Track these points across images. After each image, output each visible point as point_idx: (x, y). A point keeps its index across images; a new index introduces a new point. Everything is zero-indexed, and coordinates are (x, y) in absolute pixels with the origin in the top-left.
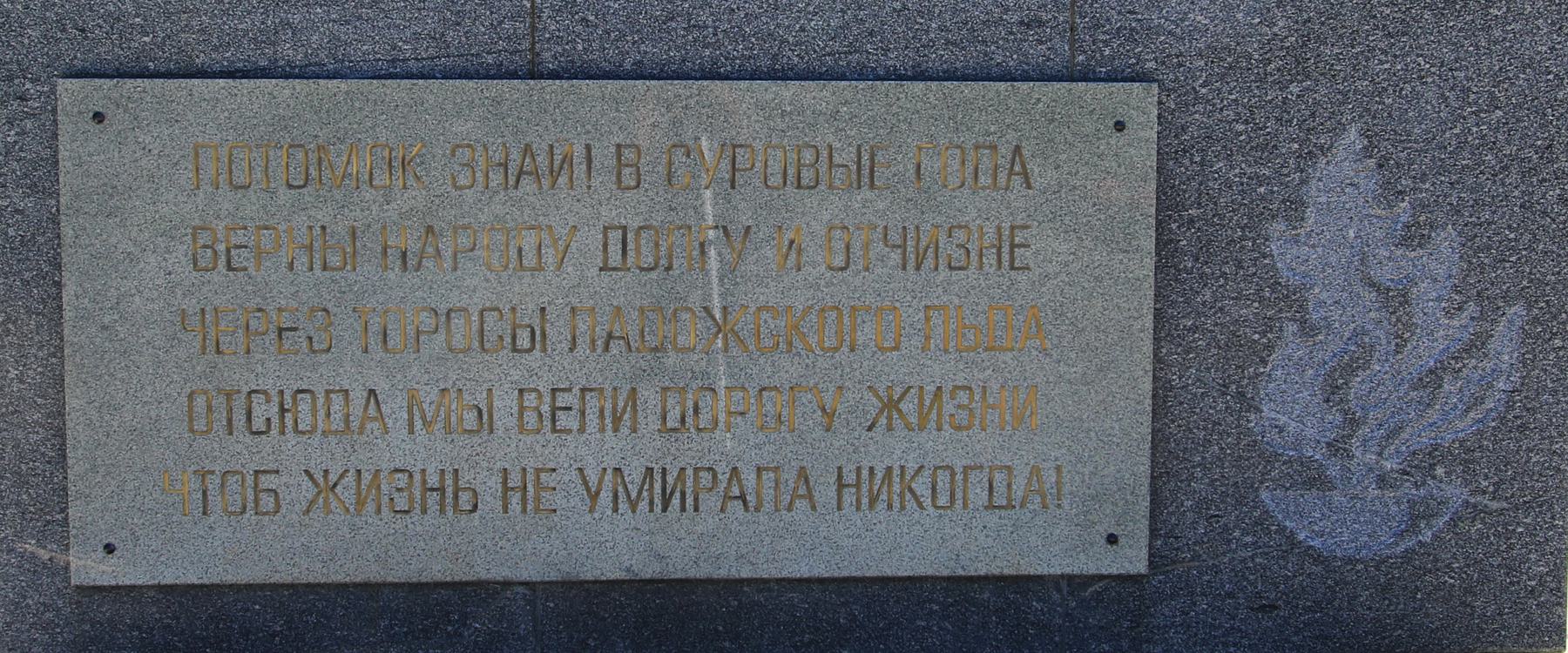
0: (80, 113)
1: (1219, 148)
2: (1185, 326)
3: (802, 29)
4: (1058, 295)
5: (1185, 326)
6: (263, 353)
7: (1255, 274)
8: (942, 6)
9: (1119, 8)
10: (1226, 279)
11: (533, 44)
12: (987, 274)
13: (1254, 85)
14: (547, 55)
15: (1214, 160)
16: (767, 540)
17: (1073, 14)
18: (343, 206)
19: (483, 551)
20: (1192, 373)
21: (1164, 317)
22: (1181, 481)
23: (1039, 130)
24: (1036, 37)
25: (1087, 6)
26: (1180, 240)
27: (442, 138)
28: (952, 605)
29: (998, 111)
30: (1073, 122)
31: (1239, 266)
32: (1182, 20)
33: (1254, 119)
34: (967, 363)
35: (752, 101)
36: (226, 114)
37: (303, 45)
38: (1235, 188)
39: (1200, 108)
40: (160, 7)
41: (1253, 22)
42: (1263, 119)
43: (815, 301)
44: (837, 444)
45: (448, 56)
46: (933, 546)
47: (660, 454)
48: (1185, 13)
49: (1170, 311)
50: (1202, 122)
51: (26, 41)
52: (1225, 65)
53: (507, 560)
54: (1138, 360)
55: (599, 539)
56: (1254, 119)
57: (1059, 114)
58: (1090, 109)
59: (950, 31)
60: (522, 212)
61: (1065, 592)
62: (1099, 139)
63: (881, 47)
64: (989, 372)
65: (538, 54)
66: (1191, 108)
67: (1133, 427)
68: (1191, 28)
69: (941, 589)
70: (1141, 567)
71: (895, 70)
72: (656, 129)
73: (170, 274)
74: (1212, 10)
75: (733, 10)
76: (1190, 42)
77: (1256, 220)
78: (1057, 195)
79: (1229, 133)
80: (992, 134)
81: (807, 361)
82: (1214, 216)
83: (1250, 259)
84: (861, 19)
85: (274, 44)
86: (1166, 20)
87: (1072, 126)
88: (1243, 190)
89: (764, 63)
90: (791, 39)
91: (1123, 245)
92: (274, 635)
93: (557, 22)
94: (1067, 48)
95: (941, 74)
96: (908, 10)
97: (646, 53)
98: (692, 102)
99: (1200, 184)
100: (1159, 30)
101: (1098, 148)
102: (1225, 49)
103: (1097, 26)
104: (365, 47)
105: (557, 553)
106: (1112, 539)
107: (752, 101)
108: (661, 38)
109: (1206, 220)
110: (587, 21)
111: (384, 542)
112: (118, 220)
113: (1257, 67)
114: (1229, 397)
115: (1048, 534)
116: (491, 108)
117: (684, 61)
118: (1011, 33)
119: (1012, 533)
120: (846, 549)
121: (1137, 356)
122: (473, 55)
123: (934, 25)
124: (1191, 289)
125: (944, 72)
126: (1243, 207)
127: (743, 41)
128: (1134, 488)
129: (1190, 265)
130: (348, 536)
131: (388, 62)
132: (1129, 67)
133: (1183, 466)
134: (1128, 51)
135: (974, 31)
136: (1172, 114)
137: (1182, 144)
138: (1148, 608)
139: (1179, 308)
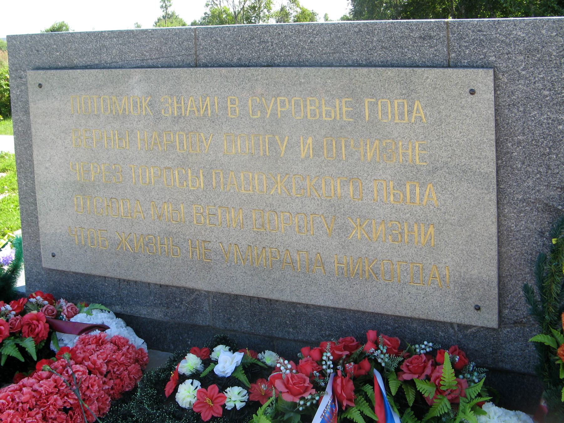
0: (34, 84)
1: (534, 104)
2: (518, 199)
3: (311, 42)
4: (443, 178)
5: (518, 199)
6: (99, 182)
7: (558, 173)
8: (379, 30)
9: (473, 29)
10: (541, 174)
11: (196, 51)
12: (405, 165)
13: (553, 69)
14: (202, 56)
15: (532, 110)
16: (304, 286)
17: (448, 32)
18: (123, 122)
19: (183, 274)
20: (522, 224)
21: (505, 193)
22: (518, 281)
23: (428, 93)
24: (428, 44)
25: (455, 28)
26: (513, 153)
27: (158, 94)
28: (397, 328)
29: (406, 83)
30: (447, 89)
31: (548, 168)
32: (509, 35)
33: (554, 88)
34: (397, 210)
35: (286, 77)
36: (81, 84)
37: (110, 55)
38: (544, 126)
39: (522, 82)
40: (62, 41)
41: (552, 35)
42: (560, 89)
43: (320, 174)
44: (334, 244)
45: (163, 57)
46: (384, 299)
47: (253, 240)
48: (511, 31)
49: (509, 190)
50: (523, 89)
51: (21, 56)
52: (536, 59)
53: (193, 279)
54: (488, 216)
55: (230, 275)
56: (554, 88)
57: (439, 85)
58: (455, 82)
59: (384, 42)
60: (191, 126)
61: (456, 330)
62: (461, 98)
63: (350, 50)
64: (408, 215)
65: (198, 56)
66: (517, 82)
67: (487, 251)
68: (515, 39)
69: (392, 319)
70: (493, 323)
71: (357, 61)
72: (244, 90)
73: (66, 148)
74: (527, 29)
75: (280, 34)
76: (514, 46)
77: (558, 143)
78: (440, 127)
79: (539, 96)
80: (403, 94)
81: (318, 202)
82: (532, 140)
83: (555, 165)
84: (339, 37)
85: (100, 54)
86: (500, 35)
87: (446, 91)
88: (549, 127)
89: (295, 58)
90: (306, 47)
91: (477, 154)
92: (112, 297)
93: (205, 42)
94: (445, 50)
95: (380, 63)
96: (362, 32)
97: (242, 54)
98: (259, 77)
99: (524, 123)
100: (496, 40)
101: (461, 103)
102: (535, 50)
103: (461, 38)
104: (132, 55)
105: (213, 279)
106: (478, 308)
107: (286, 77)
108: (248, 48)
109: (528, 143)
110: (217, 41)
111: (146, 265)
112: (48, 126)
113: (555, 59)
114: (544, 239)
115: (442, 301)
116: (176, 81)
117: (259, 58)
118: (415, 42)
119: (424, 298)
120: (341, 295)
121: (488, 214)
122: (172, 57)
123: (375, 39)
124: (521, 179)
125: (382, 62)
126: (549, 136)
127: (285, 48)
128: (489, 283)
129: (519, 166)
130: (133, 261)
131: (140, 60)
132: (480, 60)
133: (519, 273)
134: (479, 51)
135: (396, 42)
136: (506, 85)
137: (513, 101)
138: (502, 344)
139: (514, 188)
